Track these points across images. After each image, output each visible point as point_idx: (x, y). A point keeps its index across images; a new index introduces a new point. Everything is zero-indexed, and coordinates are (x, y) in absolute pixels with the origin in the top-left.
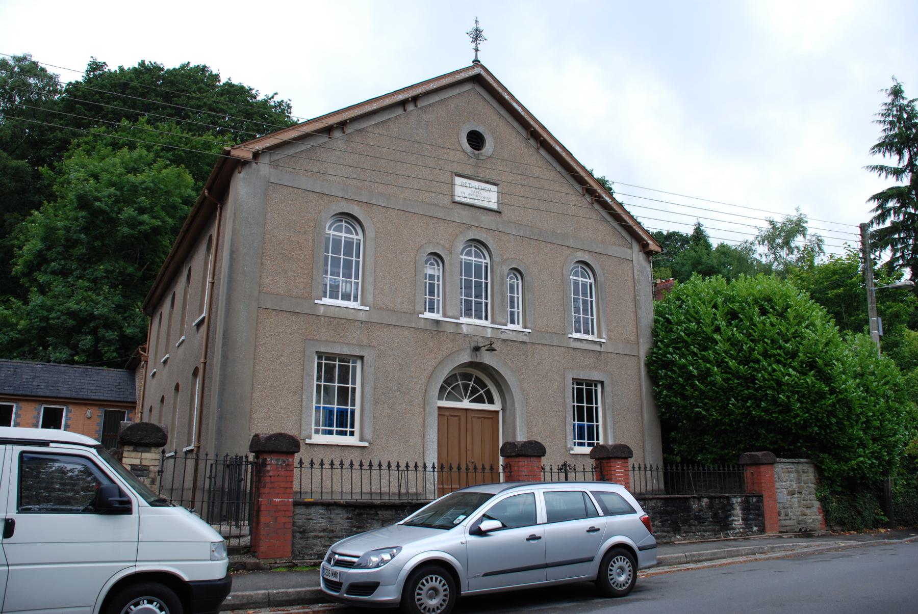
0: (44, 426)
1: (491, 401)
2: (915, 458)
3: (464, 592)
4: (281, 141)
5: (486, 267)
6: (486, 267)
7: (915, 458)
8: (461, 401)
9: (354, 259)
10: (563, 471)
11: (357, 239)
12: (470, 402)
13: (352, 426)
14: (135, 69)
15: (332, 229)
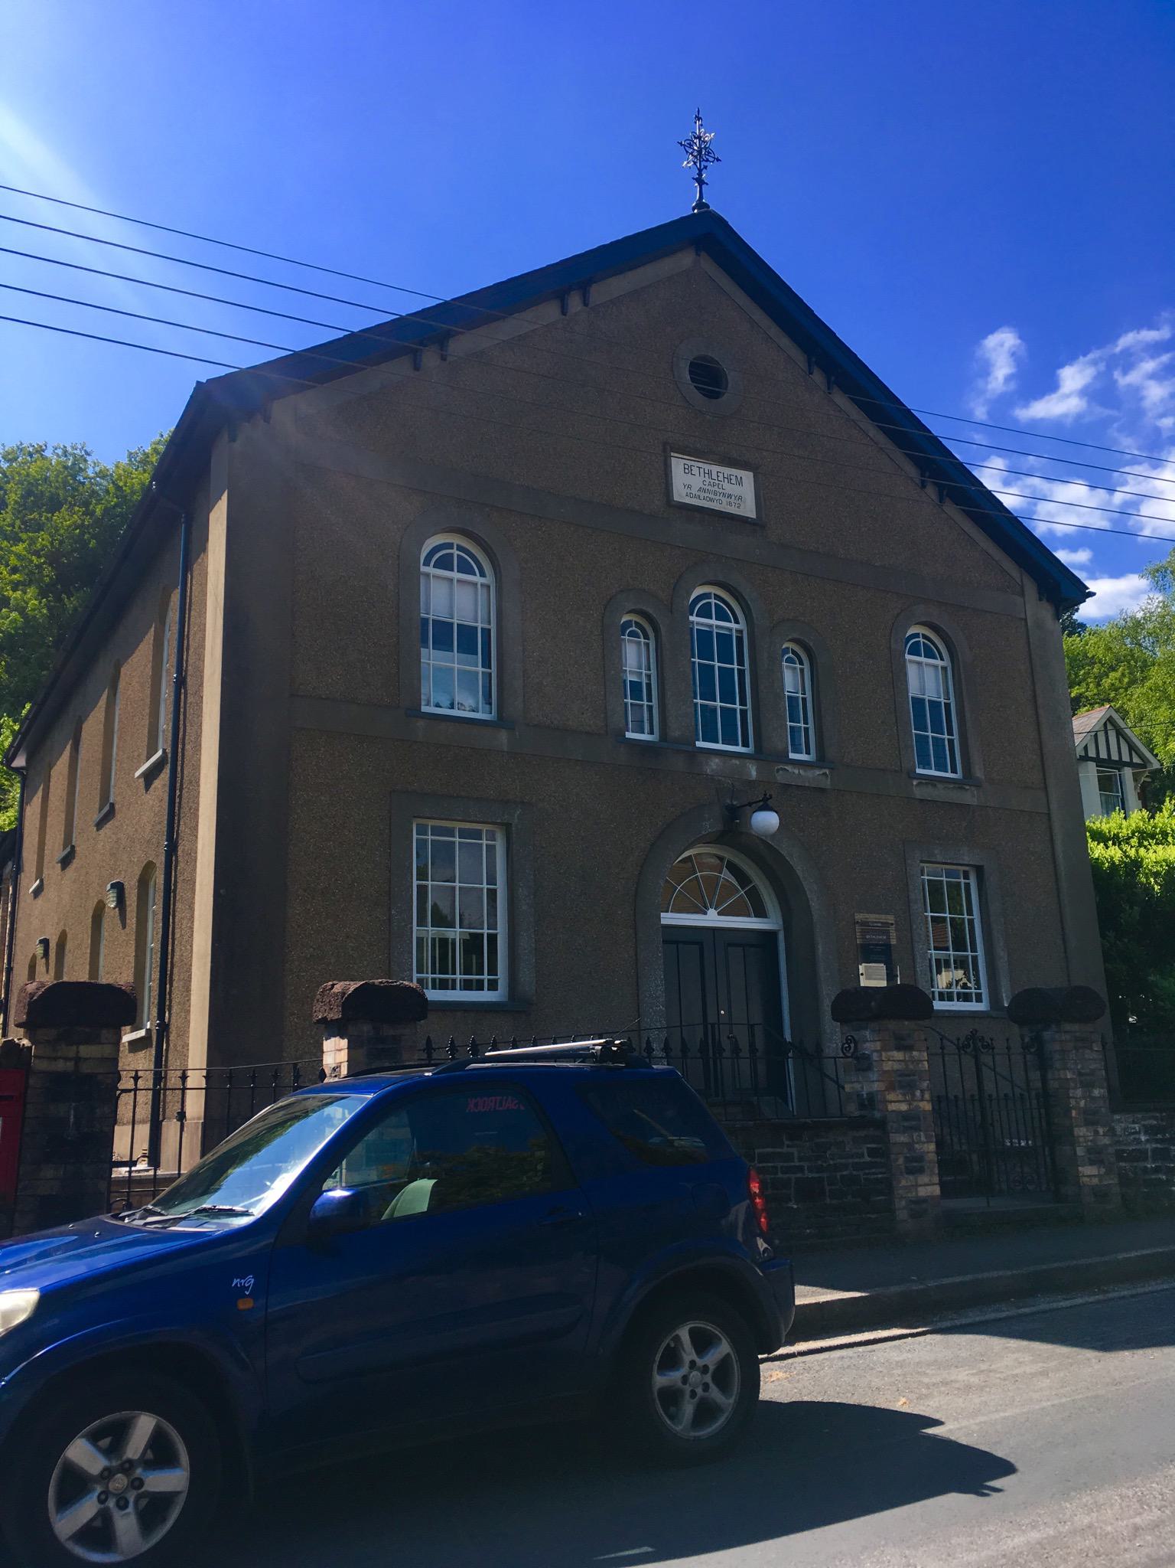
0: (417, 937)
1: (760, 912)
2: (1173, 1545)
3: (762, 1366)
4: (223, 371)
5: (740, 640)
6: (740, 640)
7: (1173, 1545)
8: (705, 913)
9: (736, 666)
10: (968, 1050)
11: (737, 631)
12: (719, 914)
13: (493, 970)
14: (1048, 601)
15: (432, 563)
